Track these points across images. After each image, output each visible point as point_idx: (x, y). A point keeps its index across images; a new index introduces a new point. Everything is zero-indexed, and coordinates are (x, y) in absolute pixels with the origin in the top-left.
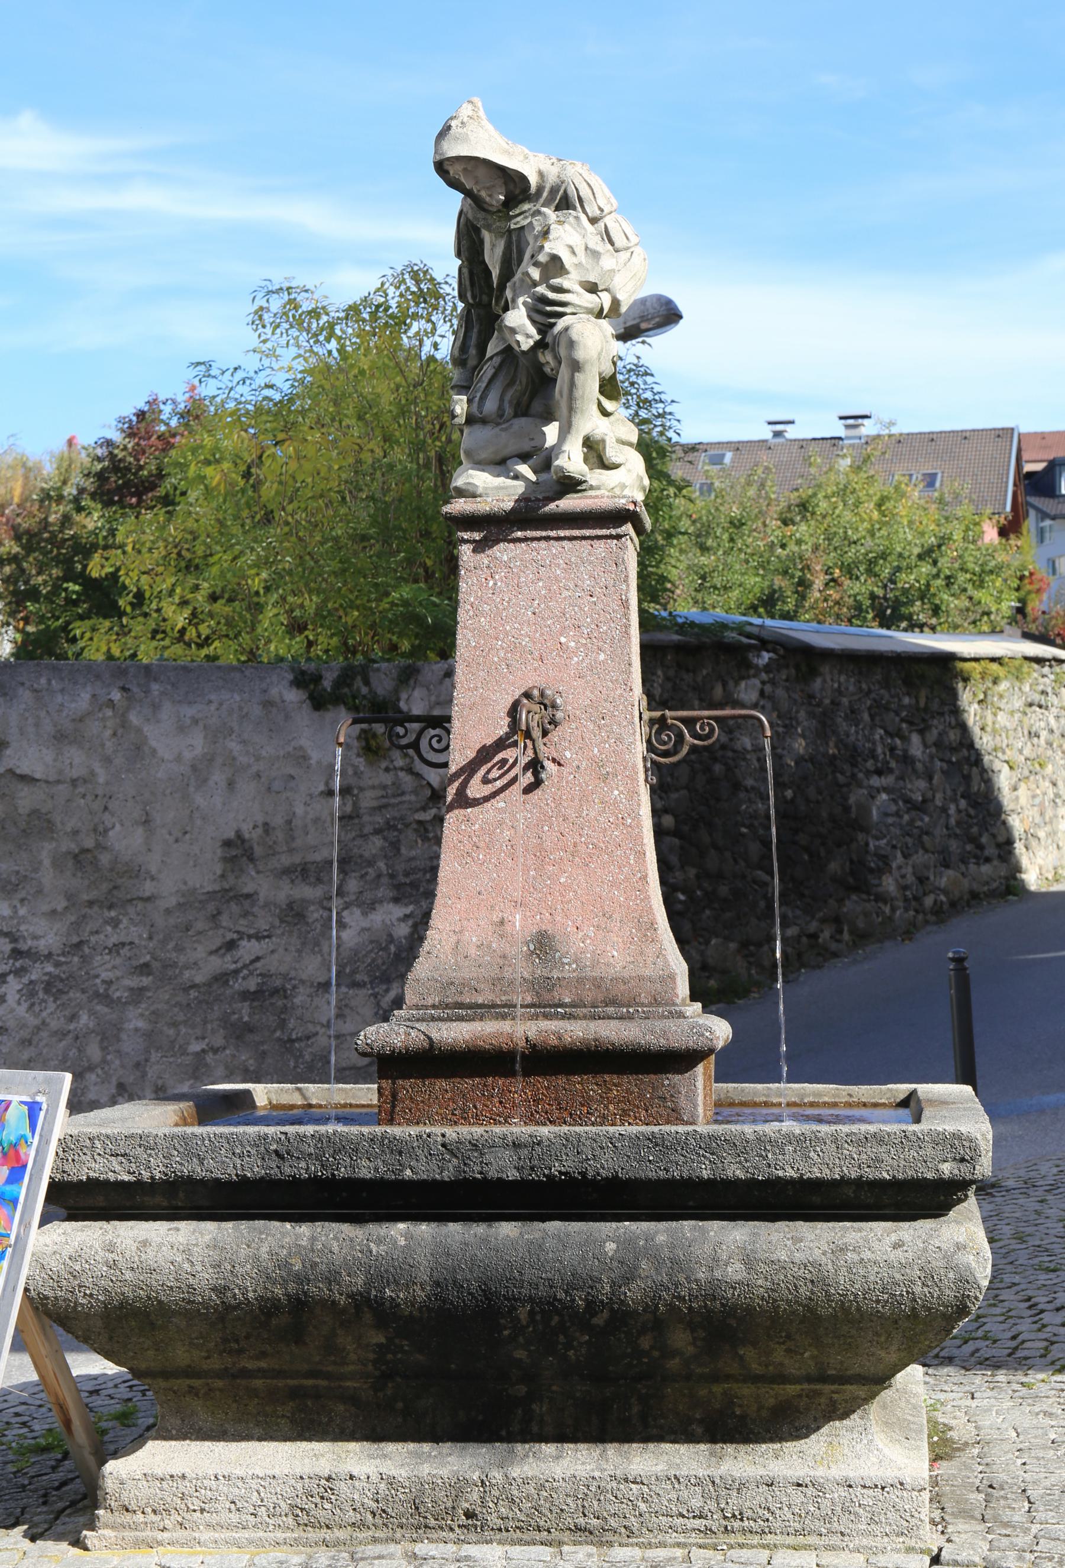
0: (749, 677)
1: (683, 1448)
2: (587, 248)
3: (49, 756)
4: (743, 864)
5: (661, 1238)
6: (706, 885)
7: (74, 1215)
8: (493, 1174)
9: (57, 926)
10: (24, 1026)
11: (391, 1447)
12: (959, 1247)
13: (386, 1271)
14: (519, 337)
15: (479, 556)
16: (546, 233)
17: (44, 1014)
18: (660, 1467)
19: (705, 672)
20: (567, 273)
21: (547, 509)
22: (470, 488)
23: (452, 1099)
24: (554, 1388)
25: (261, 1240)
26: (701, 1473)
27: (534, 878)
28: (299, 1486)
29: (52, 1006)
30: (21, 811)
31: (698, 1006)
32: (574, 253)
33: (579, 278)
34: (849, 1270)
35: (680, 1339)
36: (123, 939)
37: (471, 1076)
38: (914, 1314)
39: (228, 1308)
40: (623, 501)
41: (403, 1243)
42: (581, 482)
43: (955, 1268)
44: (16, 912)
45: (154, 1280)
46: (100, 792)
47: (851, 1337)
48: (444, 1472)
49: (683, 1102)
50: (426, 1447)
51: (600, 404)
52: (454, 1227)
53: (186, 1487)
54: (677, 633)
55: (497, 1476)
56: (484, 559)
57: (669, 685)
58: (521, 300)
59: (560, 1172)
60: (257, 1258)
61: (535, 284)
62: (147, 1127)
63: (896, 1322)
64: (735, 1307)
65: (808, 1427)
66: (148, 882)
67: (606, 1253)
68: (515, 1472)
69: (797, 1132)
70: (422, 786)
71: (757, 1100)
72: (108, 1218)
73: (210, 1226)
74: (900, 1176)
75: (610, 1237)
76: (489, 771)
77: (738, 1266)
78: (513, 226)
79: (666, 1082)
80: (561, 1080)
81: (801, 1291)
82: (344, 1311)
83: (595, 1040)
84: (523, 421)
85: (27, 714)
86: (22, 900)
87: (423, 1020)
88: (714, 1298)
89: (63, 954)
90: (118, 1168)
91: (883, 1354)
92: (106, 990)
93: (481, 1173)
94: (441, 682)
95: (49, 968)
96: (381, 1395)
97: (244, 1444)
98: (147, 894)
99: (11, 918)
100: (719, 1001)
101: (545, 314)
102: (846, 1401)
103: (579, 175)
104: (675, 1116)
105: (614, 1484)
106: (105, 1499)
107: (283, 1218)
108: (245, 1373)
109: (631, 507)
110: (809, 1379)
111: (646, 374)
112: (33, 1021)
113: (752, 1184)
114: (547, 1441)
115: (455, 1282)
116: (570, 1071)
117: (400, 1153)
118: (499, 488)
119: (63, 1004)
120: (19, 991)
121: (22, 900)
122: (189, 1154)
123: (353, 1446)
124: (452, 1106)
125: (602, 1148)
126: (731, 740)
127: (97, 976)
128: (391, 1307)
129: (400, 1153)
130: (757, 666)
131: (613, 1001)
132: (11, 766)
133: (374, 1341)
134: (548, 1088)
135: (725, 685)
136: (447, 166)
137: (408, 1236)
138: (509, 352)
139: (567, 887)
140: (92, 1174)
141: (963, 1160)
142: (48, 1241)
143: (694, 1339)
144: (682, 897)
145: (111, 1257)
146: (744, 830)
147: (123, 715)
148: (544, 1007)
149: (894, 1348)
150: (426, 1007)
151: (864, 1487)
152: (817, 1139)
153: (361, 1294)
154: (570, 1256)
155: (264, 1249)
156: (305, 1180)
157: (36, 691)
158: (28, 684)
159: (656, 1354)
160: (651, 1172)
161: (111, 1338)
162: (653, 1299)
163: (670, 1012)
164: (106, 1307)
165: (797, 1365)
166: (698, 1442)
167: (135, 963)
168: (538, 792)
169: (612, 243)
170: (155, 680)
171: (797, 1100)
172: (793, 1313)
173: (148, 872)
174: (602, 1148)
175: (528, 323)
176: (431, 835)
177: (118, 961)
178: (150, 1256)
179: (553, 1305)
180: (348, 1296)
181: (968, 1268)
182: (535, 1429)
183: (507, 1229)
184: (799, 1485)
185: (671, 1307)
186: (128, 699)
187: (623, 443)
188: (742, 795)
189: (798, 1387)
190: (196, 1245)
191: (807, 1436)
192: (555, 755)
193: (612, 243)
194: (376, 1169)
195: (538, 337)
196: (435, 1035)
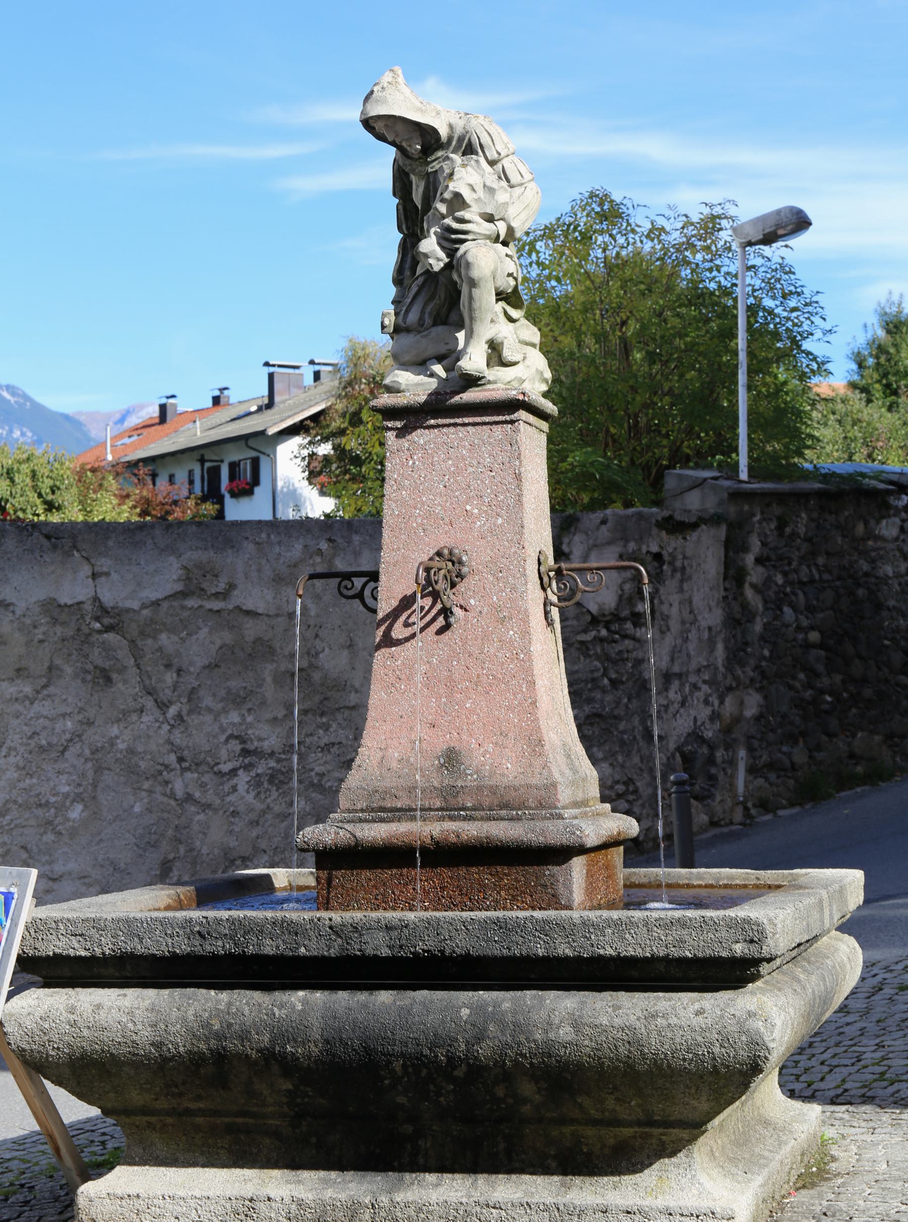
0: (889, 517)
1: (540, 1180)
2: (485, 186)
3: (269, 595)
4: (886, 670)
5: (506, 1005)
6: (851, 688)
7: (49, 983)
8: (369, 951)
9: (278, 730)
10: (252, 810)
11: (305, 1174)
12: (751, 1014)
13: (287, 1031)
14: (431, 261)
15: (400, 441)
16: (451, 175)
17: (269, 800)
18: (517, 1195)
19: (846, 513)
20: (469, 206)
21: (452, 401)
22: (395, 385)
23: (374, 886)
24: (434, 1128)
25: (189, 1004)
26: (549, 1200)
27: (445, 704)
28: (228, 1206)
29: (275, 794)
30: (247, 639)
31: (608, 806)
32: (474, 190)
33: (478, 211)
34: (659, 1033)
35: (527, 1089)
36: (332, 740)
37: (390, 868)
38: (715, 1071)
39: (165, 1060)
40: (514, 392)
41: (300, 1008)
42: (480, 378)
43: (747, 1032)
44: (244, 720)
45: (105, 1036)
46: (312, 623)
47: (666, 1089)
48: (342, 1196)
49: (561, 890)
50: (333, 1175)
51: (506, 313)
52: (342, 995)
53: (140, 1205)
54: (820, 482)
55: (384, 1200)
56: (405, 443)
57: (813, 525)
58: (432, 230)
59: (423, 950)
60: (184, 1019)
61: (444, 217)
62: (142, 909)
63: (702, 1077)
64: (567, 1063)
65: (642, 1163)
66: (353, 694)
67: (461, 1017)
68: (399, 1197)
69: (615, 917)
70: (583, 613)
71: (681, 882)
72: (73, 985)
73: (151, 993)
74: (700, 955)
75: (464, 1004)
76: (409, 617)
77: (568, 1029)
78: (430, 170)
79: (547, 873)
80: (462, 871)
81: (620, 1050)
82: (255, 1063)
83: (487, 838)
84: (440, 329)
85: (251, 562)
86: (249, 710)
87: (353, 821)
88: (550, 1056)
89: (284, 752)
90: (76, 945)
91: (695, 1103)
92: (319, 781)
93: (360, 950)
94: (598, 528)
95: (272, 764)
96: (297, 1131)
97: (190, 1170)
98: (352, 704)
99: (240, 724)
100: (865, 784)
101: (451, 241)
102: (673, 1142)
103: (482, 128)
104: (555, 902)
105: (478, 1209)
106: (78, 1214)
107: (209, 987)
108: (188, 1112)
109: (521, 397)
110: (639, 1124)
111: (791, 272)
112: (259, 806)
113: (578, 960)
114: (430, 1172)
115: (341, 1040)
116: (469, 864)
117: (296, 934)
118: (418, 385)
119: (284, 793)
120: (248, 782)
121: (249, 710)
122: (131, 934)
123: (276, 1173)
124: (375, 892)
125: (457, 930)
126: (873, 568)
127: (312, 770)
128: (292, 1061)
129: (296, 934)
130: (897, 507)
131: (506, 805)
132: (238, 603)
133: (284, 1087)
134: (451, 878)
135: (866, 523)
136: (371, 123)
137: (305, 1002)
138: (428, 273)
139: (472, 711)
140: (57, 951)
141: (752, 941)
142: (25, 1005)
143: (538, 1088)
144: (829, 699)
145: (72, 1017)
146: (887, 642)
147: (330, 561)
148: (451, 811)
149: (704, 1098)
150: (356, 811)
151: (682, 1215)
152: (631, 923)
153: (267, 1049)
154: (432, 1020)
155: (191, 1012)
156: (222, 956)
157: (258, 543)
158: (251, 538)
159: (510, 1101)
160: (497, 950)
161: (79, 1083)
162: (501, 1056)
163: (551, 814)
164: (70, 1058)
165: (627, 1112)
166: (552, 1174)
167: (342, 759)
168: (448, 633)
169: (508, 180)
170: (356, 532)
171: (714, 882)
172: (616, 1068)
173: (353, 686)
174: (457, 930)
175: (438, 249)
176: (592, 652)
177: (329, 757)
178: (102, 1017)
179: (421, 1060)
180: (258, 1051)
181: (758, 1032)
182: (421, 1161)
183: (385, 997)
184: (629, 1213)
185: (516, 1063)
186: (334, 548)
187: (527, 344)
188: (885, 613)
189: (632, 1130)
190: (138, 1008)
191: (641, 1171)
192: (462, 603)
193: (508, 180)
194: (277, 947)
195: (447, 260)
196: (359, 834)
